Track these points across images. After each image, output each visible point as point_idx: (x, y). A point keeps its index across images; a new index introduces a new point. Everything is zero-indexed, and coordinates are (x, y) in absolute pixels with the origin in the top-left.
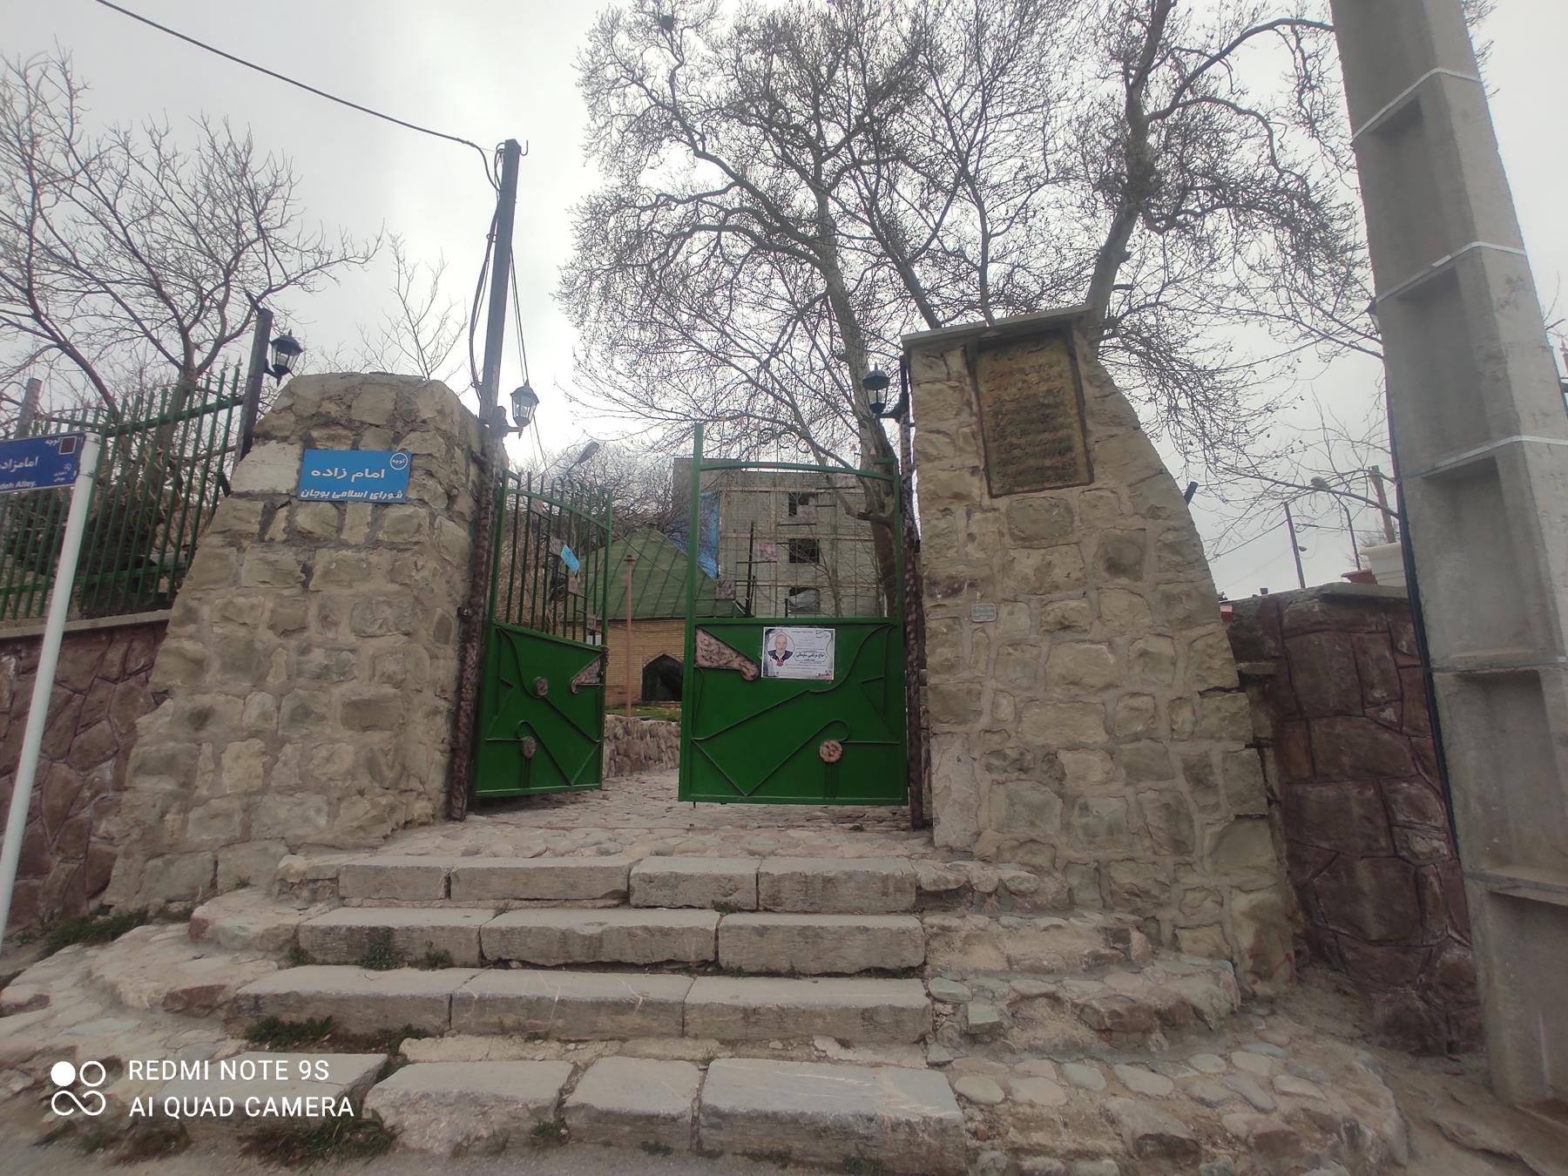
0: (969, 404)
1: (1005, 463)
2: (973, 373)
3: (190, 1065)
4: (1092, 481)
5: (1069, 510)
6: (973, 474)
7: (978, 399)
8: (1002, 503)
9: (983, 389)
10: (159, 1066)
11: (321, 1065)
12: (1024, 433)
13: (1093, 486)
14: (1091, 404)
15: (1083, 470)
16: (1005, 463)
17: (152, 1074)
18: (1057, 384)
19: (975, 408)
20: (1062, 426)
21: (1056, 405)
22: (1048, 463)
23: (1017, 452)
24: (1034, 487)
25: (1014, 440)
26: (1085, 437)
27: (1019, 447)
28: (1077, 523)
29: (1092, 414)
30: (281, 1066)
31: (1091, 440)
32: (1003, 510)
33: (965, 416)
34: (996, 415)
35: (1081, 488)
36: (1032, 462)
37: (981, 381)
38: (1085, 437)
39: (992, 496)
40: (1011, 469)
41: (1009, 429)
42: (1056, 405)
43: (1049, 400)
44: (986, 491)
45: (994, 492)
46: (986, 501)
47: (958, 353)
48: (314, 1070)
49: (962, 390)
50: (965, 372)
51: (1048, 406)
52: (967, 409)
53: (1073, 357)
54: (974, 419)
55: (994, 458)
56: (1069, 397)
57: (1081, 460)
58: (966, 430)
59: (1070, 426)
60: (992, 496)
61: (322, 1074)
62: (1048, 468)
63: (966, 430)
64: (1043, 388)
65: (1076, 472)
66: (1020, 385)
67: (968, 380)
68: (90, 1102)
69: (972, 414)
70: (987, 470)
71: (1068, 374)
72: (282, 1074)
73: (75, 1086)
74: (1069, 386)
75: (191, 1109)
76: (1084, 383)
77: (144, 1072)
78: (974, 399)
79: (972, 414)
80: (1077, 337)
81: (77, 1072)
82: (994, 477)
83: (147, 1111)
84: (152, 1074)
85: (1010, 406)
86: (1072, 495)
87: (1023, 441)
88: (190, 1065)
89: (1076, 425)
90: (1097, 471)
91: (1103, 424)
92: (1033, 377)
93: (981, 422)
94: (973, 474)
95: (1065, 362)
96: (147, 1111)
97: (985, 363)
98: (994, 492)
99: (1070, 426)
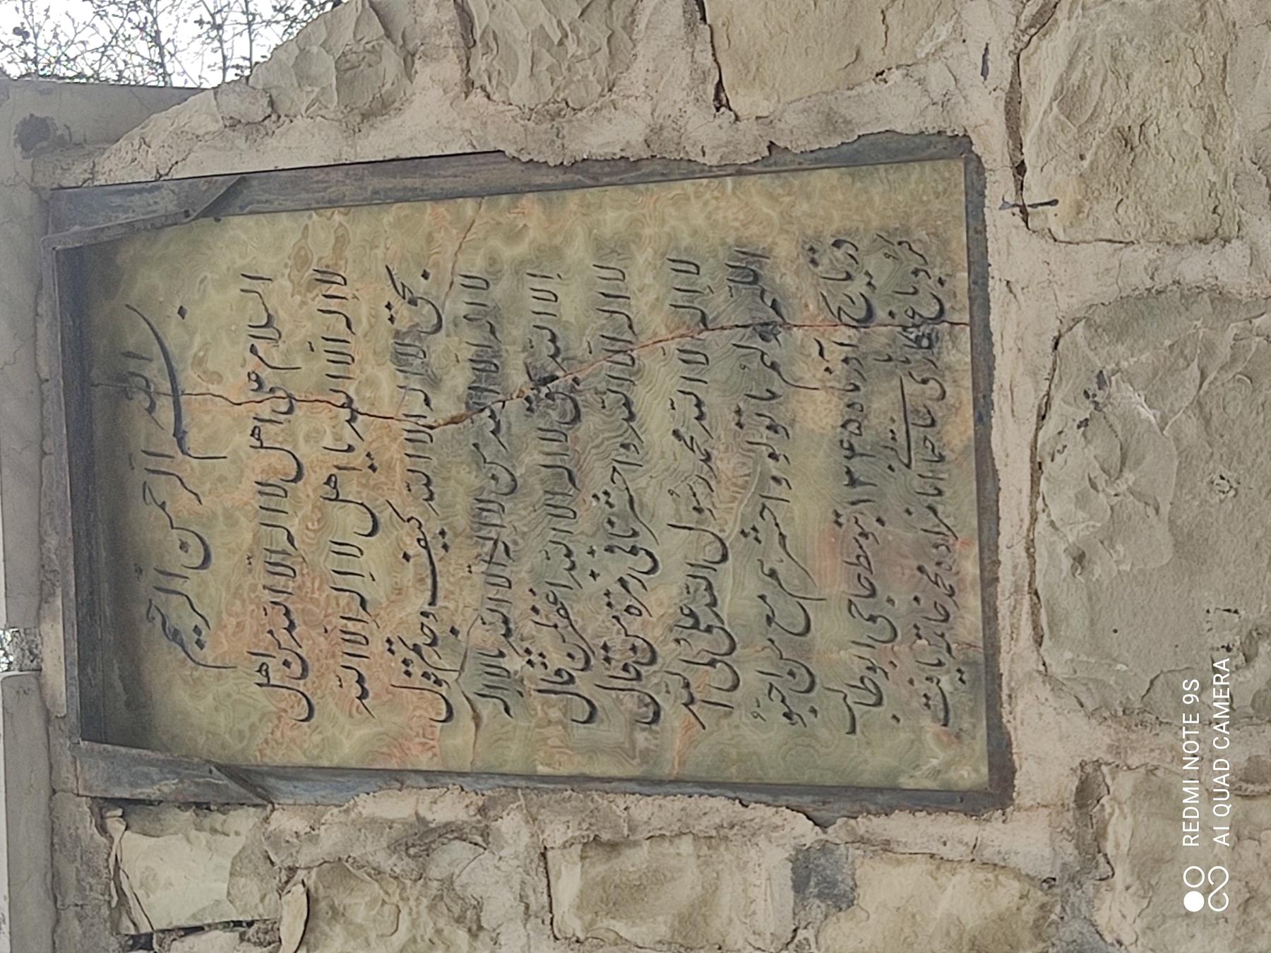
0: (421, 840)
1: (797, 684)
2: (252, 784)
3: (1188, 795)
4: (959, 146)
5: (1130, 313)
6: (840, 898)
7: (396, 778)
8: (1049, 742)
9: (348, 740)
10: (1187, 821)
11: (1187, 685)
12: (625, 531)
13: (992, 146)
14: (496, 123)
15: (882, 198)
16: (797, 684)
17: (1194, 827)
18: (367, 299)
19: (448, 808)
20: (611, 300)
21: (487, 320)
22: (817, 413)
23: (738, 594)
24: (960, 506)
25: (663, 597)
26: (688, 169)
27: (702, 577)
28: (1227, 267)
29: (556, 113)
30: (1187, 719)
31: (704, 133)
32: (1095, 740)
33: (490, 878)
34: (500, 687)
35: (1000, 222)
36: (807, 506)
37: (293, 746)
38: (688, 169)
39: (997, 793)
40: (836, 642)
41: (594, 622)
42: (487, 320)
43: (452, 353)
44: (957, 830)
45: (971, 772)
46: (1027, 838)
47: (135, 849)
48: (1191, 691)
49: (340, 869)
50: (243, 821)
51: (486, 365)
52: (452, 858)
53: (228, 197)
54: (510, 824)
55: (761, 740)
56: (455, 239)
57: (829, 201)
58: (569, 882)
59: (612, 253)
60: (997, 793)
61: (1194, 685)
62: (854, 416)
63: (569, 882)
64: (379, 383)
65: (894, 242)
66: (350, 521)
67: (287, 821)
68: (1218, 876)
69: (481, 835)
70: (823, 798)
71: (320, 232)
72: (1194, 719)
73: (1206, 890)
74: (383, 238)
75: (1224, 794)
76: (378, 143)
77: (1193, 834)
78: (397, 807)
79: (481, 835)
80: (119, 165)
81: (1193, 889)
82: (873, 757)
83: (1225, 831)
84: (1194, 827)
85: (464, 598)
86: (1037, 281)
87: (674, 549)
88: (1188, 795)
89: (613, 211)
90: (898, 110)
91: (617, 50)
92: (316, 435)
93: (533, 784)
94: (840, 898)
95: (248, 241)
96: (1225, 831)
97: (212, 702)
98: (971, 772)
99: (612, 253)
